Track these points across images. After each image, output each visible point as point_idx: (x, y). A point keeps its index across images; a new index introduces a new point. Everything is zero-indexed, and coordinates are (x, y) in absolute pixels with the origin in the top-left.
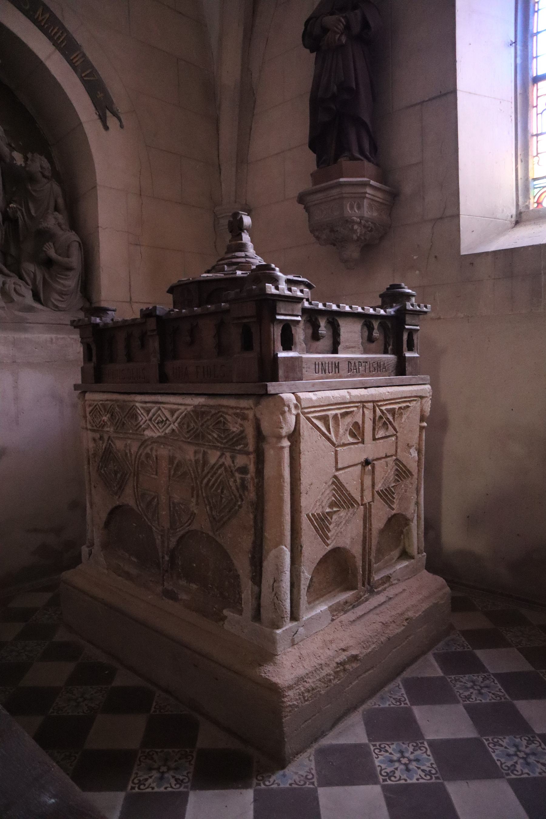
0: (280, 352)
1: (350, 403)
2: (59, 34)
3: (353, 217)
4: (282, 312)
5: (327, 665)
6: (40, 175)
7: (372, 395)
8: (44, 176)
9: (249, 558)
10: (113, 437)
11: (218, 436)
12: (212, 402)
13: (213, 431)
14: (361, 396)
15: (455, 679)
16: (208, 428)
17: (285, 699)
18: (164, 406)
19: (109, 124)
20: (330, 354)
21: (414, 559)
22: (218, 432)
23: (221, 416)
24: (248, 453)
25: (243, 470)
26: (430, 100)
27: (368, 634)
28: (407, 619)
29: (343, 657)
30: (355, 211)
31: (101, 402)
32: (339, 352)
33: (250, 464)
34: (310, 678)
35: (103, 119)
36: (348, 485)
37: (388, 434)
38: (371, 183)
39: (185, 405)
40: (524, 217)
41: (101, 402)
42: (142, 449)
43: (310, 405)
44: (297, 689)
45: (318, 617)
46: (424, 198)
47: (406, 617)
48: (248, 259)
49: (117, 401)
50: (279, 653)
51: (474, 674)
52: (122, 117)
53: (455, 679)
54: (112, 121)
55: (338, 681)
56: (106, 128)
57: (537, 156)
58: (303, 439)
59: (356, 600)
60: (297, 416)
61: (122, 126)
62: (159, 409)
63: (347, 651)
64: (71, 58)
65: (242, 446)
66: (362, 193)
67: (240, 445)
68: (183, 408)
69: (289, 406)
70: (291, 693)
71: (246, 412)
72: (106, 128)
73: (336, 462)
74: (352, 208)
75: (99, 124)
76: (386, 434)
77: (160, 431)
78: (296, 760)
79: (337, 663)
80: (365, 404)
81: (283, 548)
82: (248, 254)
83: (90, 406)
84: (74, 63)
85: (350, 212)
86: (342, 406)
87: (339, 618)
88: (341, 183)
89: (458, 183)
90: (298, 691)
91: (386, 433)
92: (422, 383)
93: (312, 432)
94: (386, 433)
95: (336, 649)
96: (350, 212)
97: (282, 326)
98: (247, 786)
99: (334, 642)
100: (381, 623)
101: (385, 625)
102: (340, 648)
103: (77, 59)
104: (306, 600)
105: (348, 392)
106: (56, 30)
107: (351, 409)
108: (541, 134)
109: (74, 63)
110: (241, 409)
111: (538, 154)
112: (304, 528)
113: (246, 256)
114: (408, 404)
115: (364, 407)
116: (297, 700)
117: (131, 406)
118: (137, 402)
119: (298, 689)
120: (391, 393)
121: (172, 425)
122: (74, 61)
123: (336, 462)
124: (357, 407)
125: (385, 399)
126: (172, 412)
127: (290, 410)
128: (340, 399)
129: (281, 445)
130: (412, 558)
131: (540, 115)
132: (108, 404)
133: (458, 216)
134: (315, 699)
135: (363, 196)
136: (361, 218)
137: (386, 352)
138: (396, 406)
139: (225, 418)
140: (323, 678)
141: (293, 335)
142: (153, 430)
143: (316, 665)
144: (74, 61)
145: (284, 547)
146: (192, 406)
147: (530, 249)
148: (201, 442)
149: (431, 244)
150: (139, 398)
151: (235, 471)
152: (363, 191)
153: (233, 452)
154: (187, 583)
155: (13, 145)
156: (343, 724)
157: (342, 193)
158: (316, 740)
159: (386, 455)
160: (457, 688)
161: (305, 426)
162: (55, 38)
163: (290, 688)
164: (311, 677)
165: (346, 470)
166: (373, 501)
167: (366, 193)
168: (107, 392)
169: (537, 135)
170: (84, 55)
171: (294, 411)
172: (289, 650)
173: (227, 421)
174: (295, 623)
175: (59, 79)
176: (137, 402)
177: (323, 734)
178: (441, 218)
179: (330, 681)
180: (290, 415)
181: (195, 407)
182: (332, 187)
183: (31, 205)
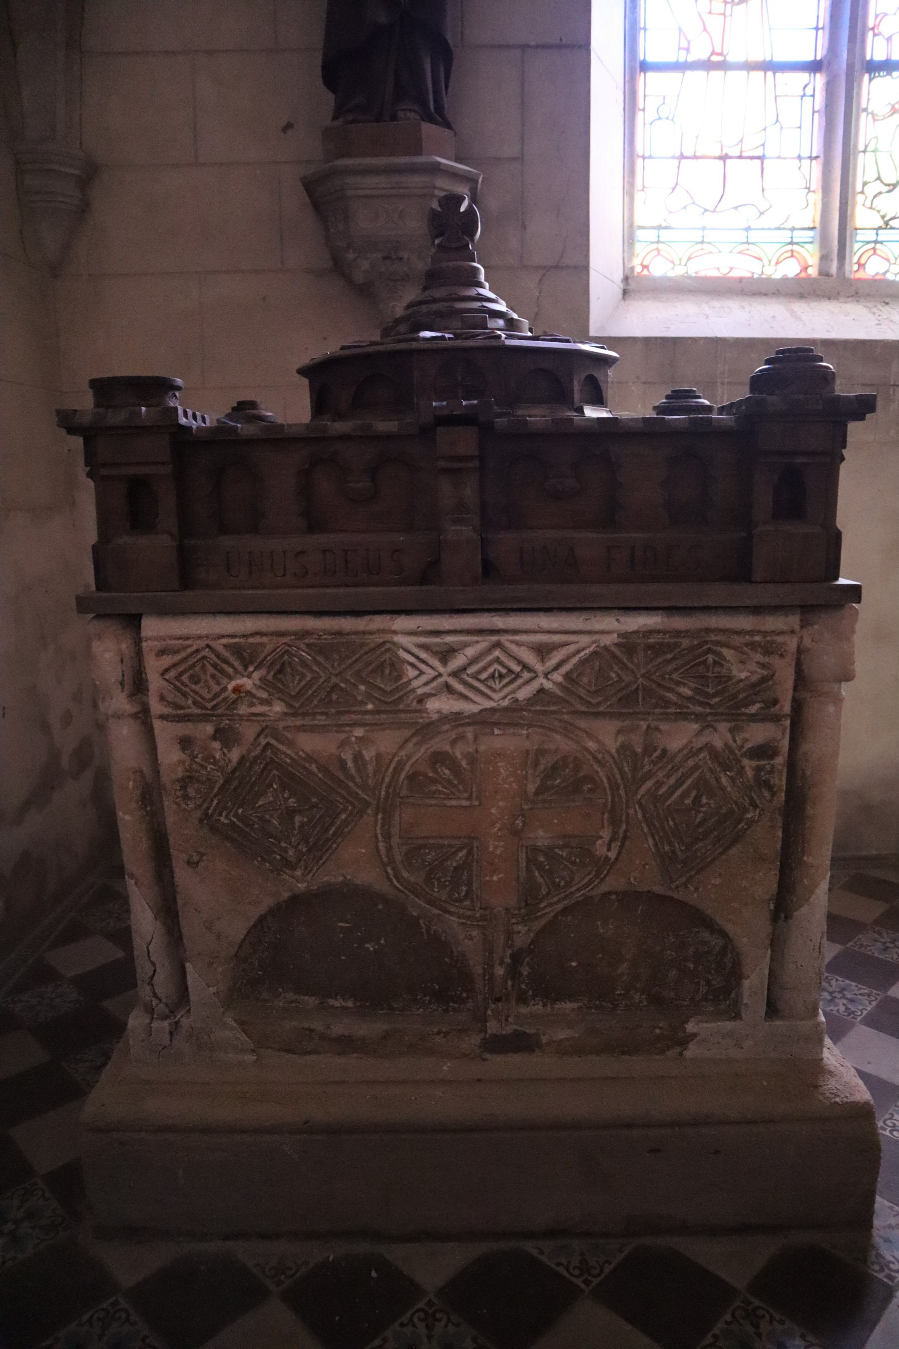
9: (771, 910)
10: (286, 728)
11: (695, 690)
12: (680, 623)
13: (678, 683)
16: (664, 679)
18: (517, 638)
22: (694, 683)
23: (709, 651)
24: (776, 719)
25: (764, 751)
26: (537, 47)
31: (225, 641)
33: (783, 738)
39: (590, 632)
40: (633, 285)
41: (225, 641)
42: (410, 745)
46: (524, 227)
49: (304, 634)
51: (873, 988)
57: (643, 190)
62: (498, 645)
65: (758, 705)
67: (754, 703)
68: (584, 640)
71: (780, 639)
77: (496, 696)
83: (161, 653)
88: (441, 167)
89: (588, 212)
108: (650, 157)
110: (764, 633)
111: (644, 187)
117: (373, 645)
118: (395, 632)
121: (542, 680)
126: (542, 651)
131: (863, 154)
132: (263, 645)
133: (585, 268)
139: (719, 654)
142: (405, 694)
146: (615, 635)
147: (702, 342)
148: (640, 708)
149: (536, 310)
150: (402, 623)
151: (741, 756)
153: (734, 720)
154: (545, 1005)
157: (435, 187)
168: (266, 612)
169: (644, 157)
173: (725, 659)
176: (395, 632)
178: (556, 267)
181: (623, 635)
182: (413, 170)
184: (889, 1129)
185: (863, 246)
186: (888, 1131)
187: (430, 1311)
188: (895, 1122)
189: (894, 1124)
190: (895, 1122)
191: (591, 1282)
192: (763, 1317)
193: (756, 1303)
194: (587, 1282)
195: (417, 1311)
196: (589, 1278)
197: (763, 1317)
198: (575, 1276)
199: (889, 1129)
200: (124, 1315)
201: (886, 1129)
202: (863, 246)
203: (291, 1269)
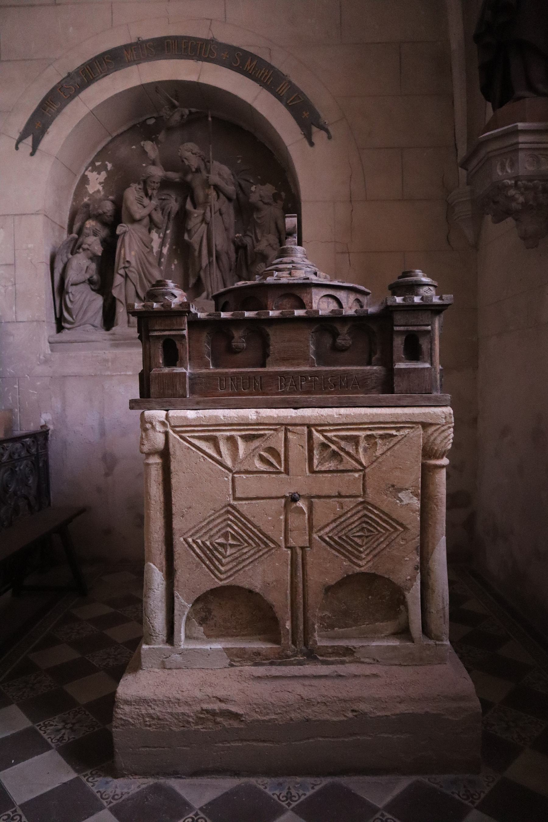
0: (400, 360)
1: (330, 425)
2: (266, 74)
3: (505, 179)
4: (157, 328)
5: (186, 703)
6: (260, 204)
7: (303, 417)
8: (265, 203)
14: (278, 417)
15: (45, 724)
17: (119, 711)
19: (315, 139)
20: (258, 367)
21: (413, 642)
27: (270, 699)
28: (353, 711)
29: (216, 706)
30: (507, 172)
32: (267, 365)
34: (158, 706)
35: (308, 136)
36: (256, 519)
37: (341, 467)
38: (519, 128)
43: (185, 424)
44: (136, 709)
45: (207, 654)
47: (355, 708)
48: (293, 265)
50: (144, 669)
52: (330, 129)
53: (45, 724)
54: (318, 136)
55: (201, 728)
56: (312, 144)
58: (175, 458)
59: (277, 656)
60: (166, 434)
61: (330, 137)
63: (226, 704)
64: (277, 91)
66: (512, 145)
69: (151, 423)
70: (127, 708)
72: (312, 144)
73: (319, 497)
74: (503, 168)
75: (306, 143)
76: (337, 468)
78: (131, 779)
79: (202, 710)
80: (289, 427)
81: (150, 566)
82: (295, 259)
84: (280, 95)
85: (500, 174)
86: (246, 427)
87: (242, 667)
90: (137, 710)
91: (338, 466)
92: (425, 404)
93: (189, 453)
94: (338, 466)
95: (209, 694)
96: (500, 174)
97: (162, 342)
98: (77, 771)
99: (214, 687)
100: (299, 696)
101: (309, 703)
102: (214, 695)
103: (281, 91)
104: (203, 631)
105: (257, 412)
106: (263, 72)
107: (262, 432)
109: (280, 95)
112: (179, 552)
113: (293, 262)
114: (394, 432)
115: (286, 430)
116: (132, 718)
119: (138, 709)
120: (347, 416)
122: (280, 92)
123: (319, 497)
124: (275, 430)
125: (331, 422)
127: (153, 427)
128: (236, 419)
129: (147, 462)
130: (412, 640)
134: (161, 730)
135: (515, 149)
136: (517, 179)
137: (369, 363)
138: (362, 434)
140: (178, 714)
141: (178, 350)
143: (170, 696)
144: (280, 92)
145: (152, 564)
152: (515, 141)
155: (252, 181)
156: (209, 780)
158: (167, 775)
159: (339, 494)
160: (48, 735)
161: (177, 446)
162: (262, 79)
163: (127, 702)
164: (159, 705)
165: (254, 502)
166: (310, 546)
167: (518, 143)
170: (290, 82)
171: (159, 428)
172: (157, 670)
174: (168, 647)
175: (264, 114)
177: (176, 774)
179: (188, 722)
180: (154, 433)
183: (258, 231)
184: (12, 815)
185: (131, 281)
186: (11, 813)
187: (289, 800)
188: (486, 780)
189: (487, 778)
190: (486, 780)
191: (287, 804)
192: (463, 795)
193: (466, 802)
194: (289, 804)
195: (296, 801)
196: (381, 817)
197: (463, 795)
198: (390, 819)
199: (12, 815)
200: (53, 741)
201: (13, 813)
202: (131, 281)
203: (295, 797)
